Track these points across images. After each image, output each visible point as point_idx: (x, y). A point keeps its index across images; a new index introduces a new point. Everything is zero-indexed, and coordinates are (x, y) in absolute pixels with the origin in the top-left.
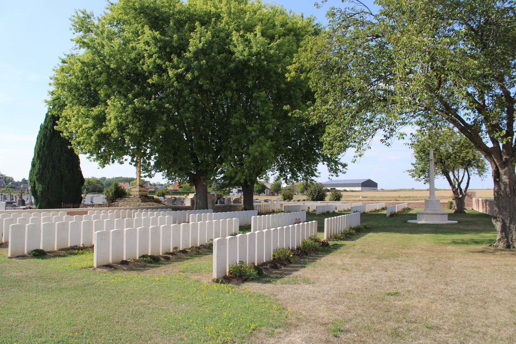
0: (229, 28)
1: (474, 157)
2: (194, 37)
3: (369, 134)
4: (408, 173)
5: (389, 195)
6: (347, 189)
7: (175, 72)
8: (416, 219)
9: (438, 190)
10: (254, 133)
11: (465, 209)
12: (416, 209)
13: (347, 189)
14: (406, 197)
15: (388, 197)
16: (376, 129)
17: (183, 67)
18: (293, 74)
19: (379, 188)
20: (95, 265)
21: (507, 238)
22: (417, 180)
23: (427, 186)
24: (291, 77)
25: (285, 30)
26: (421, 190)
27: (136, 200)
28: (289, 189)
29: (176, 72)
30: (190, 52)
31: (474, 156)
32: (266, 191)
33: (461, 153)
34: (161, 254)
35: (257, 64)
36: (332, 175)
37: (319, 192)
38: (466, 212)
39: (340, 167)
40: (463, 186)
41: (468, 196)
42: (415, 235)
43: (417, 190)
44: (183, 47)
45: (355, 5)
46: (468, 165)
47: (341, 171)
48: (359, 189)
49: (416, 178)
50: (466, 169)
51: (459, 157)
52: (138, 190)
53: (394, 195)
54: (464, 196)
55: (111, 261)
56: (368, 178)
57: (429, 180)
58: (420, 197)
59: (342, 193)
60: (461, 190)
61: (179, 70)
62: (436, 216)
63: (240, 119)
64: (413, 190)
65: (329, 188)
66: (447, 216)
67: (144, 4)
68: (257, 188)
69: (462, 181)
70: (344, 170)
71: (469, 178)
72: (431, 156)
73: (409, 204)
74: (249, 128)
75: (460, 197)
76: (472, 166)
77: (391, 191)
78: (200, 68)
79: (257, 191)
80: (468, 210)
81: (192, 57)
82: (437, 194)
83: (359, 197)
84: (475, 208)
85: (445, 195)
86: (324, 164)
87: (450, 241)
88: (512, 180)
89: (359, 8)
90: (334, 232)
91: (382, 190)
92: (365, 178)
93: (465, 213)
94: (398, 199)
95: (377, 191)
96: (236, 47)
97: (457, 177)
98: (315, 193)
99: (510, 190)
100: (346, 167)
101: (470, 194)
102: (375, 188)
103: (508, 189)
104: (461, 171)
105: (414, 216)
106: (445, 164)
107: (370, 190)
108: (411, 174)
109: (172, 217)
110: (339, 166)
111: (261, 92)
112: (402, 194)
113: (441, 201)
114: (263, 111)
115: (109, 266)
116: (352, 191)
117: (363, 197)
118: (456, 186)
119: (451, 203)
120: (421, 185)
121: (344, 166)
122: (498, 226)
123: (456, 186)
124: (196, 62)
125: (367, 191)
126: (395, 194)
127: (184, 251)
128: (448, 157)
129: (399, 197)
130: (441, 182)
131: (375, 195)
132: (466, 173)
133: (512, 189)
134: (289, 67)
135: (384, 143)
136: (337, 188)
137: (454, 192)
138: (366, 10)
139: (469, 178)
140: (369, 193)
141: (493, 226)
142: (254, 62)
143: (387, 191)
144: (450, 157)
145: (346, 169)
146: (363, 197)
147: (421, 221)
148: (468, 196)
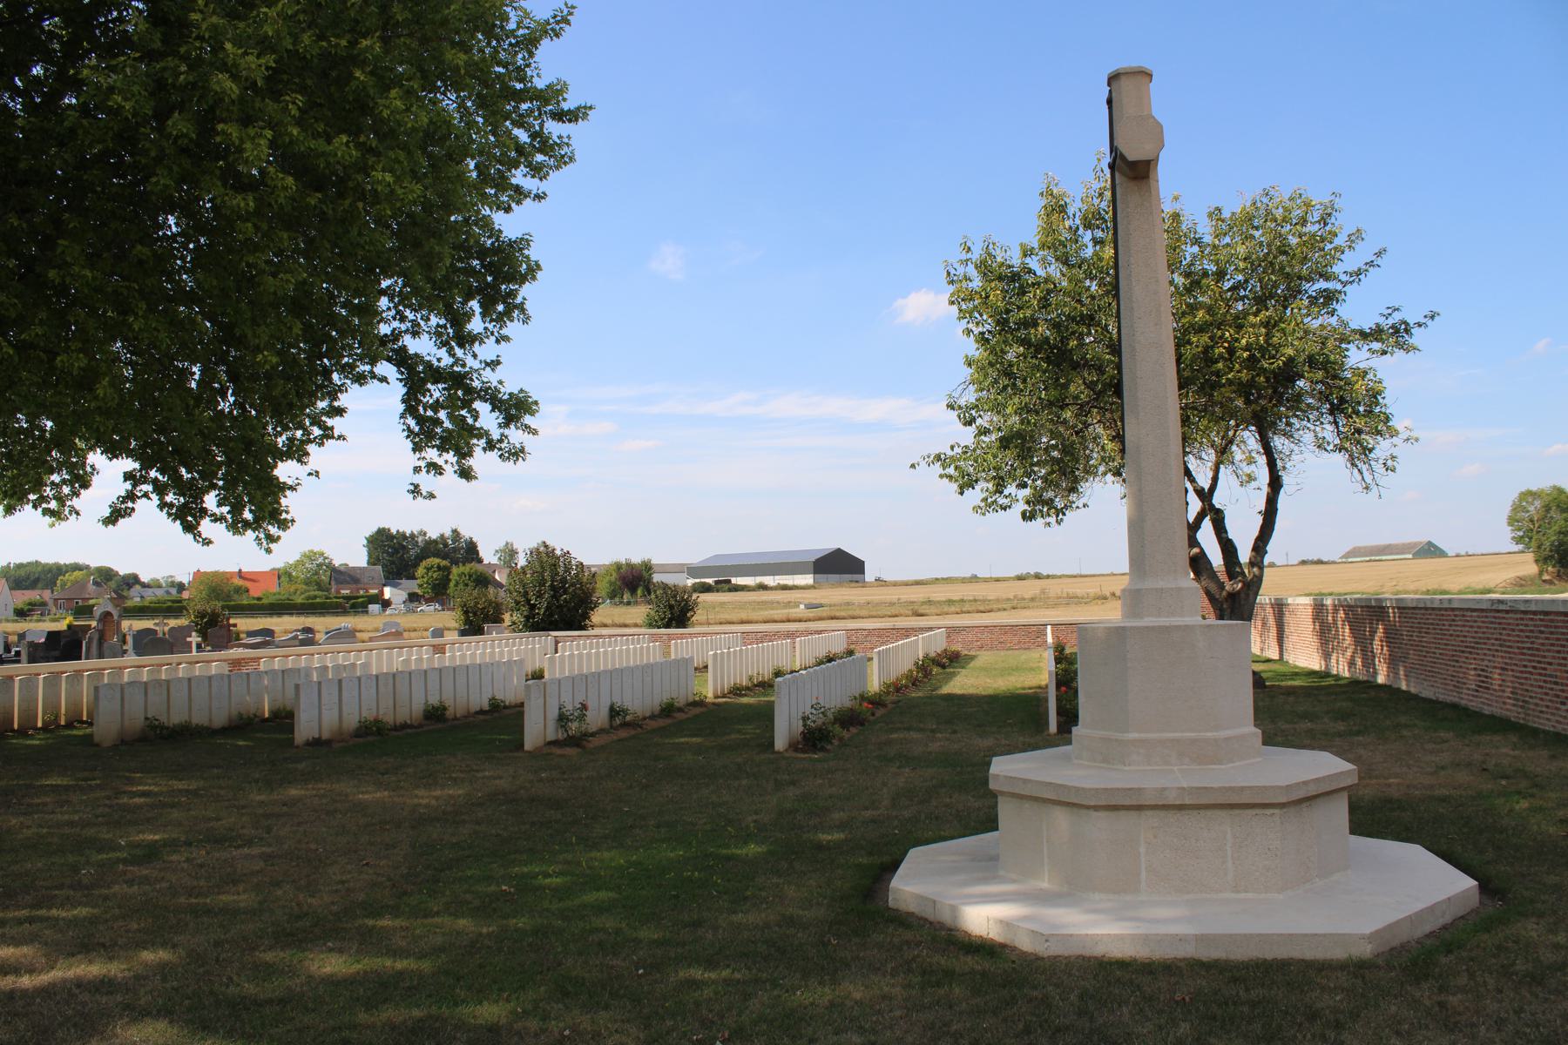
5: (894, 598)
6: (769, 580)
9: (1131, 172)
13: (769, 580)
14: (950, 602)
15: (892, 604)
19: (869, 576)
26: (997, 580)
34: (710, 695)
36: (434, 468)
39: (488, 418)
43: (986, 580)
47: (491, 446)
48: (808, 579)
51: (1231, 351)
53: (913, 597)
58: (998, 600)
62: (1226, 827)
64: (974, 579)
65: (710, 581)
70: (515, 436)
73: (952, 631)
92: (827, 544)
95: (864, 584)
100: (527, 419)
102: (856, 577)
107: (840, 584)
110: (482, 407)
112: (939, 593)
116: (785, 588)
117: (809, 607)
121: (515, 409)
125: (833, 586)
126: (918, 594)
129: (929, 602)
131: (847, 598)
140: (837, 593)
143: (895, 584)
145: (527, 429)
146: (809, 607)
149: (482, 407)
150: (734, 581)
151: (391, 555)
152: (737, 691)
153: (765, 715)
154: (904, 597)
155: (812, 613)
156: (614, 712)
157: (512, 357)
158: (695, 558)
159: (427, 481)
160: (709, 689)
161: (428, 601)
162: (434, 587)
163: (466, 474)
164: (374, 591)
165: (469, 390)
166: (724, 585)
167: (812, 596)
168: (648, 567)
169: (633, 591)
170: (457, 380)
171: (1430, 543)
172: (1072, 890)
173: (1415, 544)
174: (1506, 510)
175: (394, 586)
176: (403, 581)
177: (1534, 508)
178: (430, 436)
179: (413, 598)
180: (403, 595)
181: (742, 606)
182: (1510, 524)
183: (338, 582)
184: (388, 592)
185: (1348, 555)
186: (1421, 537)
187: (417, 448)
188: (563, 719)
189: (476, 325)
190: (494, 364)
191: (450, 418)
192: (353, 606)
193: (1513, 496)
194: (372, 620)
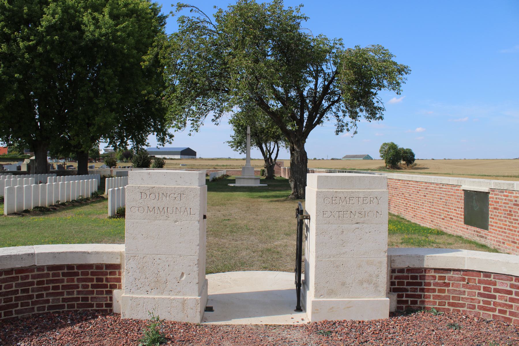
0: (78, 5)
2: (47, 13)
3: (203, 113)
4: (228, 144)
5: (207, 164)
6: (167, 157)
7: (27, 44)
8: (235, 183)
9: (252, 159)
10: (100, 106)
11: (274, 176)
12: (233, 176)
13: (167, 157)
14: (223, 166)
15: (207, 165)
16: (209, 111)
17: (34, 40)
18: (147, 63)
19: (198, 156)
20: (6, 213)
21: (297, 192)
22: (235, 150)
23: (244, 156)
24: (145, 66)
25: (128, 10)
26: (237, 160)
28: (107, 156)
29: (27, 43)
30: (42, 26)
33: (272, 128)
34: (47, 206)
35: (106, 45)
37: (144, 160)
38: (275, 178)
40: (273, 156)
41: (277, 165)
43: (233, 159)
44: (34, 19)
45: (200, 15)
46: (278, 139)
48: (178, 157)
49: (234, 148)
50: (276, 142)
54: (274, 165)
55: (16, 211)
56: (186, 146)
57: (245, 150)
60: (271, 159)
61: (31, 43)
62: (250, 180)
63: (88, 92)
64: (229, 159)
66: (259, 180)
69: (273, 152)
71: (278, 150)
72: (249, 131)
73: (227, 171)
74: (96, 101)
75: (271, 164)
76: (280, 140)
77: (209, 159)
80: (277, 176)
81: (44, 32)
84: (283, 176)
85: (258, 164)
89: (202, 18)
91: (201, 159)
93: (274, 179)
94: (216, 167)
95: (196, 159)
96: (86, 26)
97: (269, 149)
98: (141, 160)
99: (301, 160)
100: (173, 138)
101: (279, 163)
104: (273, 143)
106: (260, 138)
107: (189, 159)
108: (230, 144)
109: (34, 179)
110: (167, 136)
111: (107, 69)
112: (220, 163)
113: (255, 169)
114: (109, 86)
115: (15, 214)
116: (172, 159)
118: (268, 156)
119: (263, 171)
120: (237, 155)
121: (171, 136)
123: (268, 156)
124: (48, 37)
125: (187, 159)
127: (63, 204)
128: (262, 131)
129: (217, 165)
130: (256, 153)
131: (194, 163)
132: (276, 145)
134: (144, 57)
135: (214, 123)
136: (157, 156)
137: (265, 161)
138: (208, 20)
139: (278, 150)
142: (104, 42)
143: (206, 159)
144: (263, 132)
148: (277, 165)
154: (211, 164)
169: (127, 159)
171: (368, 155)
173: (364, 155)
174: (379, 148)
177: (386, 148)
182: (380, 152)
185: (344, 158)
186: (366, 153)
193: (381, 144)
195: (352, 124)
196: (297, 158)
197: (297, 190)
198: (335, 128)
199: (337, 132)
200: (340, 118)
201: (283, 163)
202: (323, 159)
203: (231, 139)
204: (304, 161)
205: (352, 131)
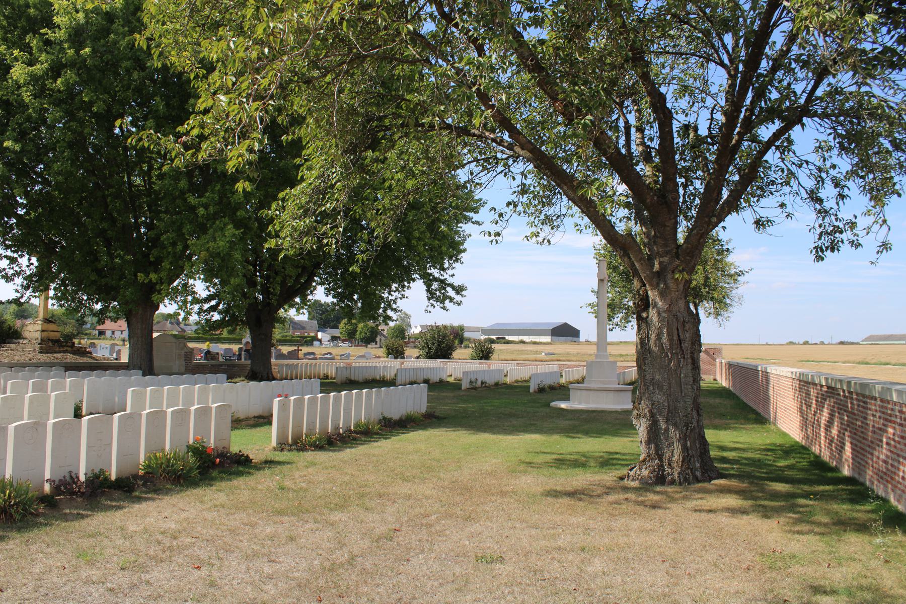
1: (705, 281)
4: (589, 309)
6: (526, 339)
8: (567, 398)
13: (526, 339)
14: (621, 355)
19: (582, 338)
21: (660, 457)
27: (30, 347)
31: (707, 278)
32: (378, 339)
37: (440, 343)
39: (451, 292)
42: (500, 437)
48: (548, 339)
52: (39, 328)
56: (563, 321)
59: (494, 345)
62: (605, 393)
65: (494, 337)
67: (737, 213)
68: (363, 334)
70: (458, 298)
78: (77, 64)
79: (362, 340)
82: (611, 350)
83: (541, 353)
86: (409, 288)
87: (549, 458)
88: (675, 316)
90: (311, 424)
92: (559, 320)
95: (579, 343)
98: (433, 344)
99: (671, 340)
100: (463, 293)
102: (575, 339)
103: (665, 339)
105: (562, 391)
107: (566, 342)
110: (449, 289)
116: (535, 343)
121: (459, 290)
122: (642, 427)
131: (568, 351)
133: (676, 337)
140: (563, 347)
141: (632, 427)
146: (547, 354)
147: (575, 403)
149: (449, 289)
150: (507, 338)
151: (321, 315)
152: (517, 381)
153: (529, 387)
155: (547, 358)
156: (482, 383)
157: (457, 273)
158: (486, 324)
159: (430, 309)
160: (508, 380)
161: (344, 341)
162: (349, 334)
163: (444, 308)
164: (312, 334)
165: (446, 284)
166: (502, 340)
167: (550, 349)
168: (462, 328)
170: (442, 281)
172: (580, 403)
175: (324, 332)
176: (328, 329)
178: (433, 297)
179: (334, 338)
180: (329, 337)
181: (512, 352)
183: (294, 328)
184: (320, 335)
185: (866, 340)
187: (429, 299)
188: (471, 382)
189: (446, 265)
190: (452, 276)
191: (439, 293)
192: (306, 342)
194: (316, 348)
195: (870, 220)
196: (659, 336)
197: (658, 449)
198: (811, 240)
199: (819, 254)
200: (827, 205)
201: (720, 350)
202: (822, 343)
203: (593, 299)
204: (686, 345)
205: (870, 243)
